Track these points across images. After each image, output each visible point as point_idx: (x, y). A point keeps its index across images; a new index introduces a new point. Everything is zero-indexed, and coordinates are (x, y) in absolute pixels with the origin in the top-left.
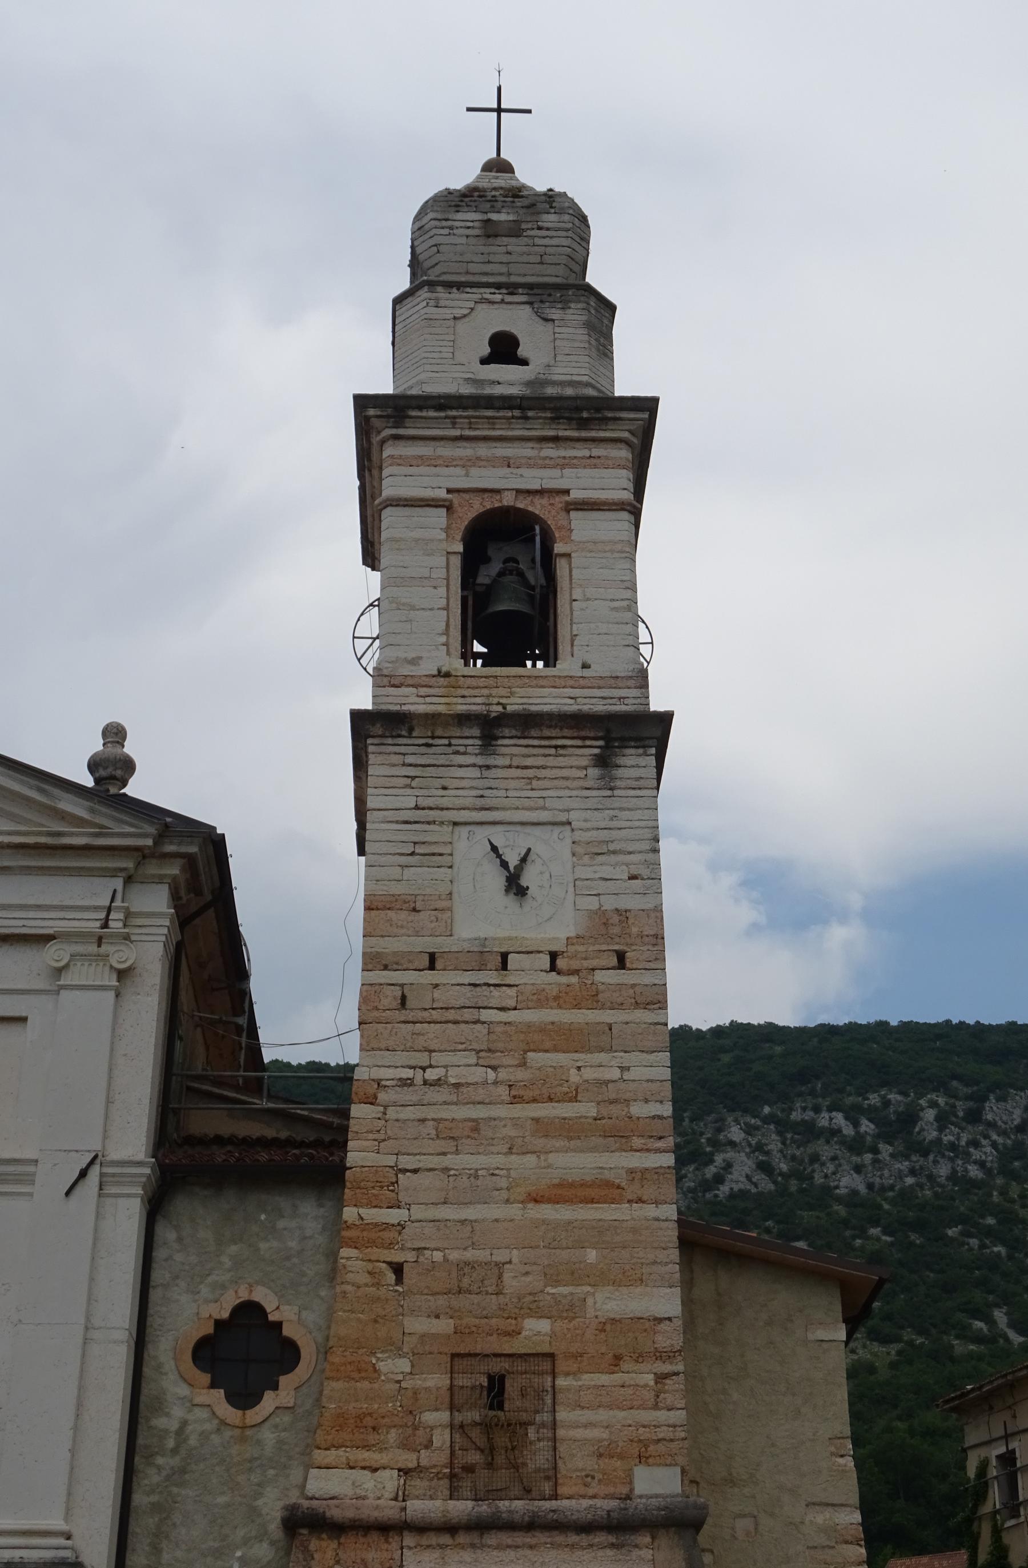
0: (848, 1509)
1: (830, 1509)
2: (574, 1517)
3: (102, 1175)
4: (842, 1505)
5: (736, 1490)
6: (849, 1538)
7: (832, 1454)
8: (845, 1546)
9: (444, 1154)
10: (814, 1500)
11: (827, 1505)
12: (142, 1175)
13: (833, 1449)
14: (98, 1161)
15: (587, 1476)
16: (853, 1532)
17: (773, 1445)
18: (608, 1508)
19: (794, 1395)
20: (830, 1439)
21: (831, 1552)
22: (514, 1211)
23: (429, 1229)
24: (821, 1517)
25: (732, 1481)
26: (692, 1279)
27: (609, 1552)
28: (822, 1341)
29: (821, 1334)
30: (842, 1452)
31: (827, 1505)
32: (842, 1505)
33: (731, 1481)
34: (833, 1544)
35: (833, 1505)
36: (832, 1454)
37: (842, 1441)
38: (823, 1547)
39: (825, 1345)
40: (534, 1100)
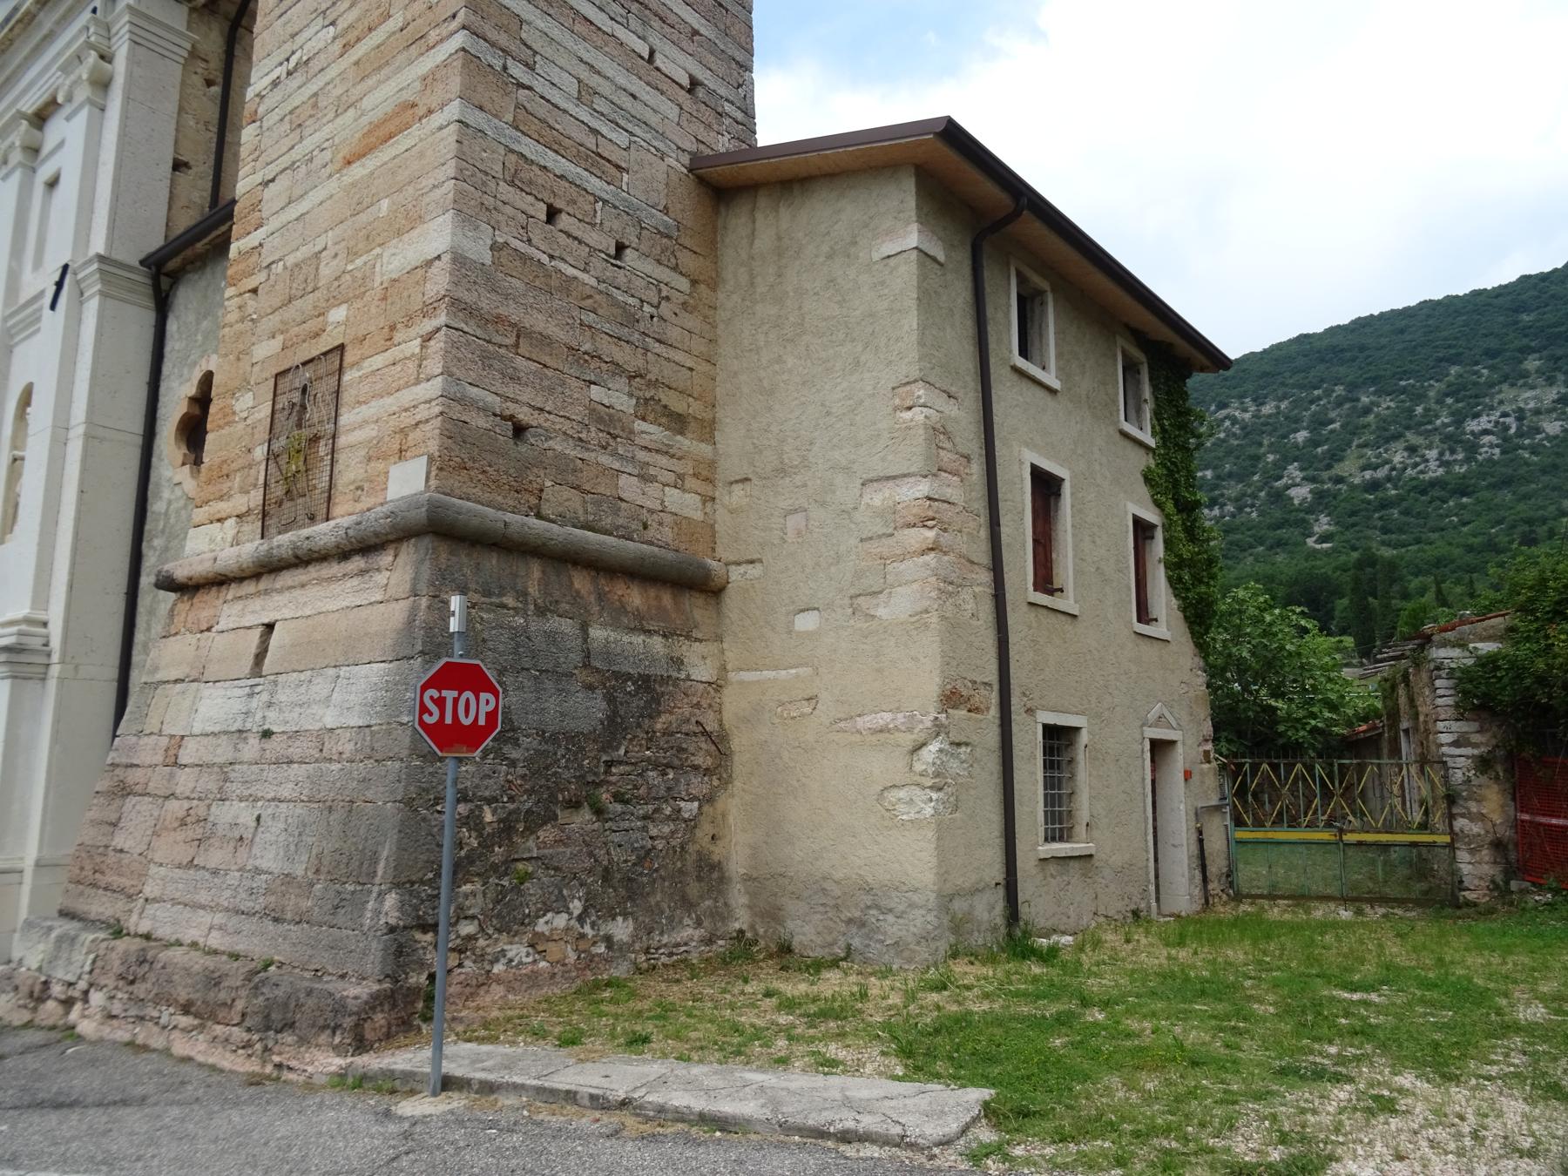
0: (912, 480)
1: (891, 484)
2: (322, 543)
3: (78, 282)
4: (905, 476)
5: (788, 480)
6: (911, 519)
7: (896, 409)
8: (906, 531)
9: (293, 147)
10: (870, 476)
11: (888, 478)
12: (92, 274)
13: (897, 401)
14: (70, 271)
15: (357, 489)
16: (915, 511)
17: (828, 414)
18: (346, 525)
19: (853, 340)
20: (893, 389)
21: (891, 541)
22: (332, 186)
23: (277, 240)
24: (878, 497)
25: (783, 470)
26: (754, 231)
27: (355, 581)
28: (889, 257)
29: (889, 248)
30: (909, 403)
31: (888, 478)
32: (905, 476)
33: (782, 471)
34: (890, 531)
35: (894, 478)
36: (896, 409)
37: (908, 388)
38: (880, 537)
39: (892, 262)
40: (359, 40)
